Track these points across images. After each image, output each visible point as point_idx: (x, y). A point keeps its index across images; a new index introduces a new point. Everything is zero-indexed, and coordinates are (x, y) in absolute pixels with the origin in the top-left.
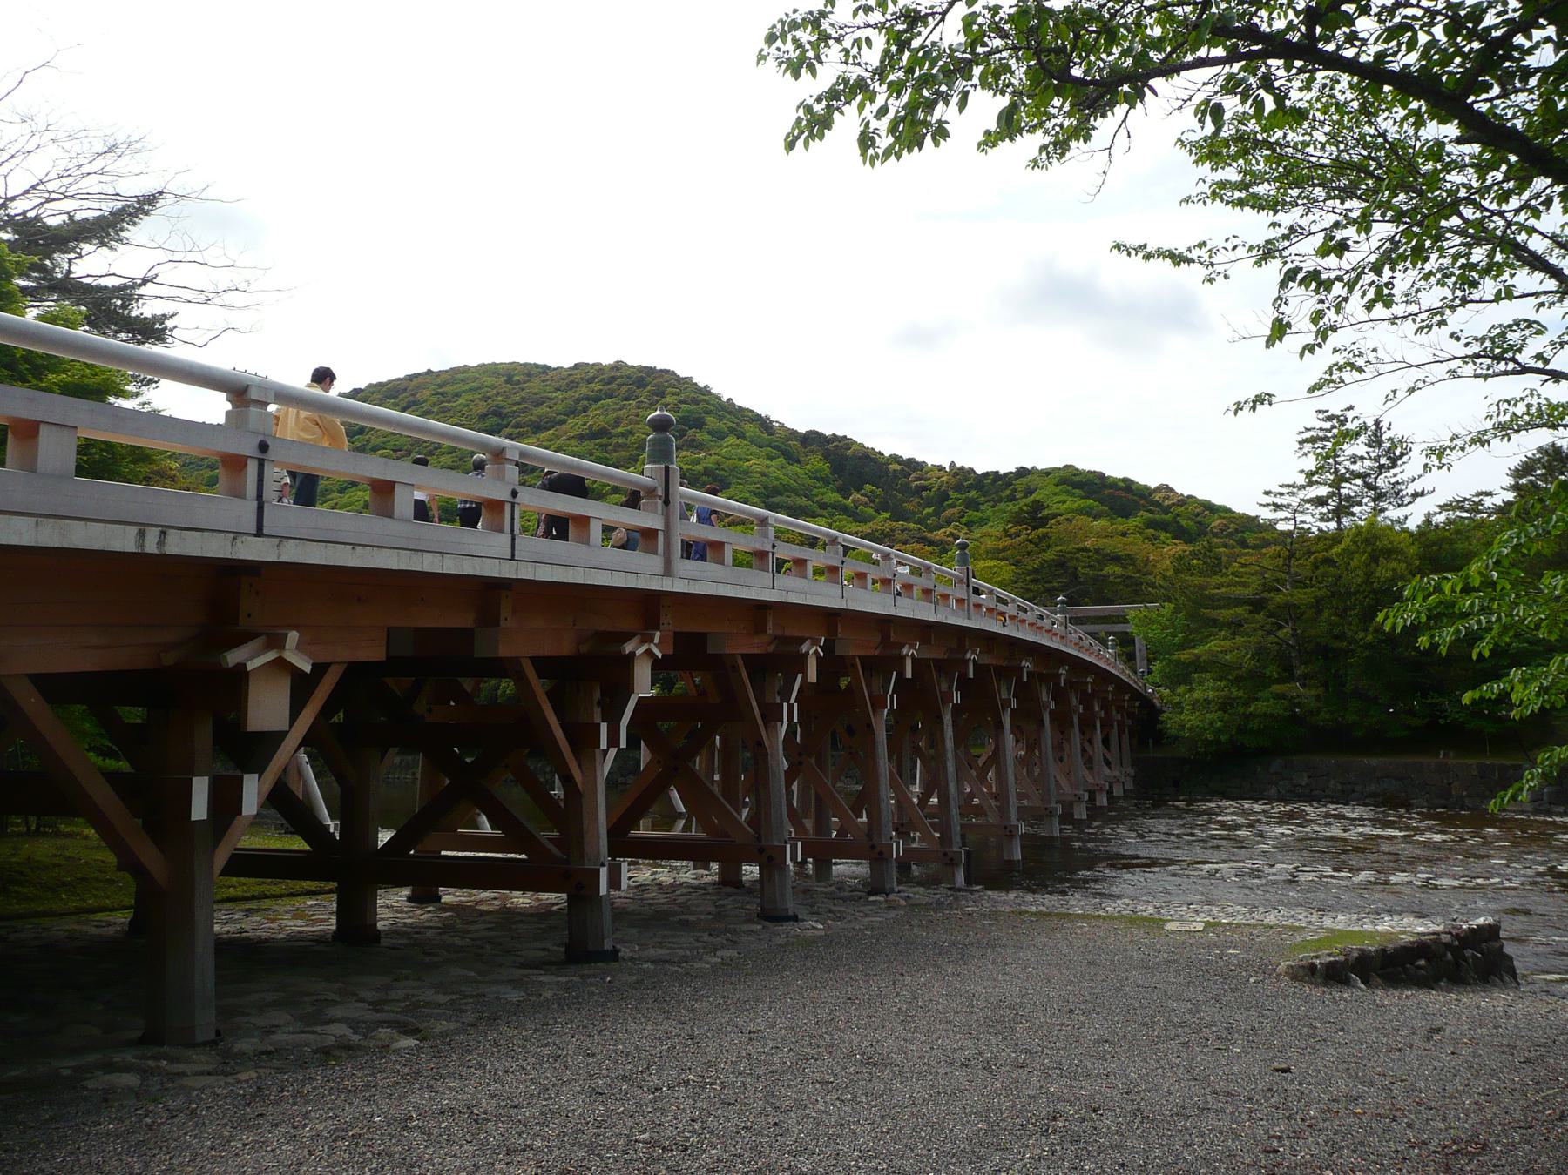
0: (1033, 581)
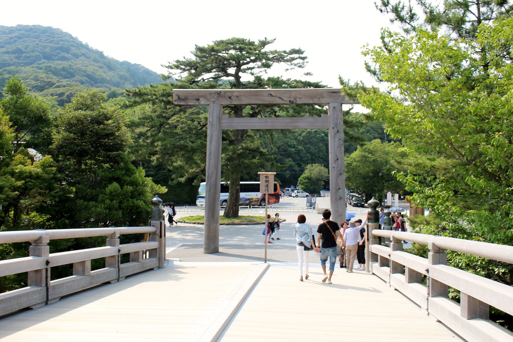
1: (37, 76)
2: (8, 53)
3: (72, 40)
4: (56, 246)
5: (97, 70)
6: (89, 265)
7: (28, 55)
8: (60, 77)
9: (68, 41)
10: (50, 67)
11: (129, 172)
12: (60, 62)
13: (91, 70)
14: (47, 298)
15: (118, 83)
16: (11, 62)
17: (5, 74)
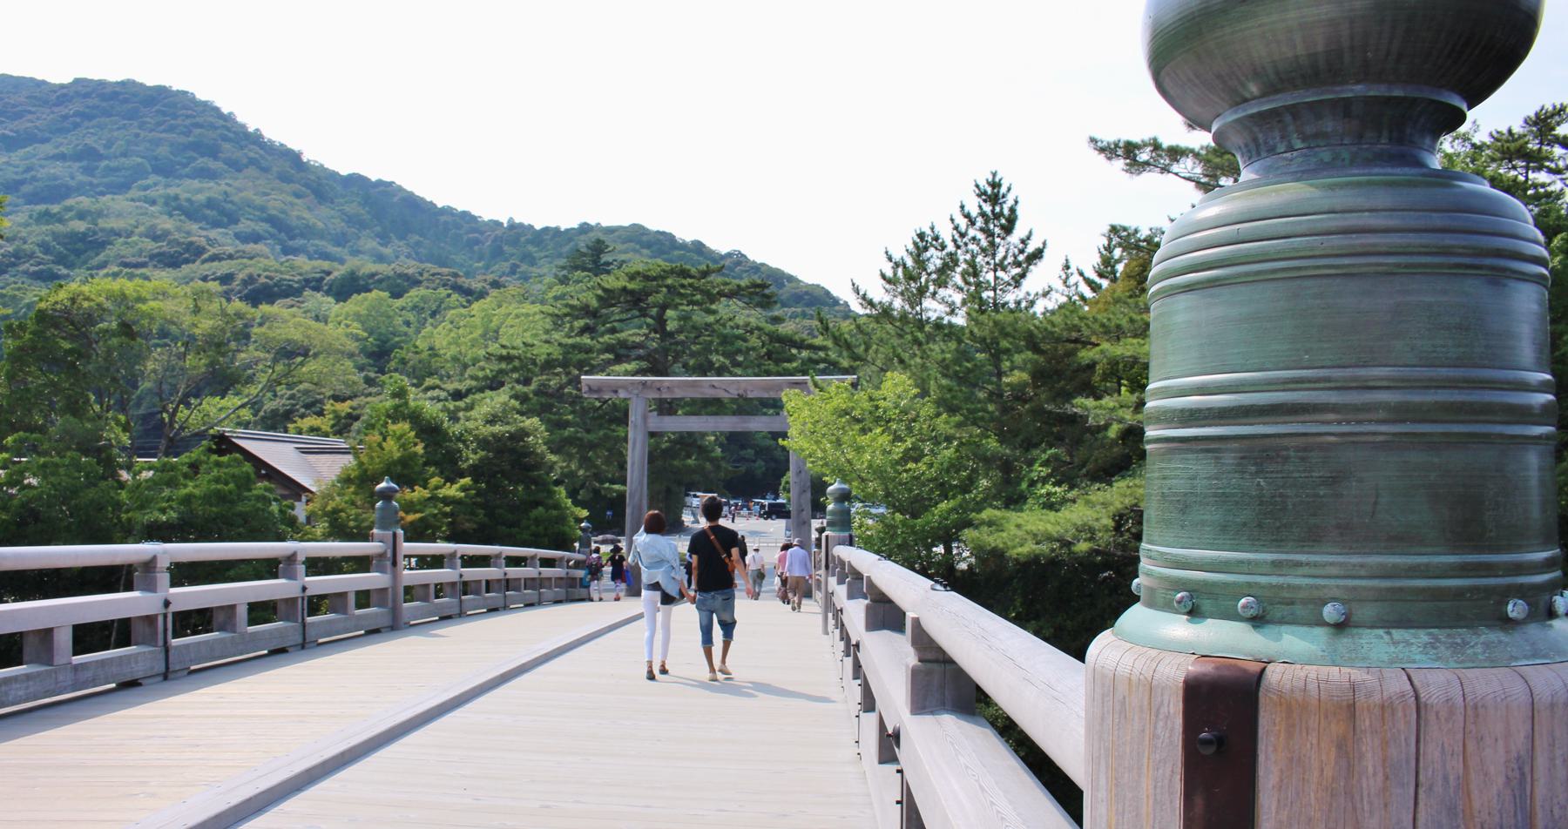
0: (585, 330)
1: (153, 227)
2: (62, 157)
3: (221, 122)
4: (186, 573)
5: (292, 204)
6: (242, 612)
7: (114, 164)
8: (203, 224)
9: (213, 127)
10: (176, 198)
11: (551, 493)
12: (196, 184)
13: (278, 204)
14: (167, 668)
15: (344, 234)
16: (73, 183)
17: (71, 219)
